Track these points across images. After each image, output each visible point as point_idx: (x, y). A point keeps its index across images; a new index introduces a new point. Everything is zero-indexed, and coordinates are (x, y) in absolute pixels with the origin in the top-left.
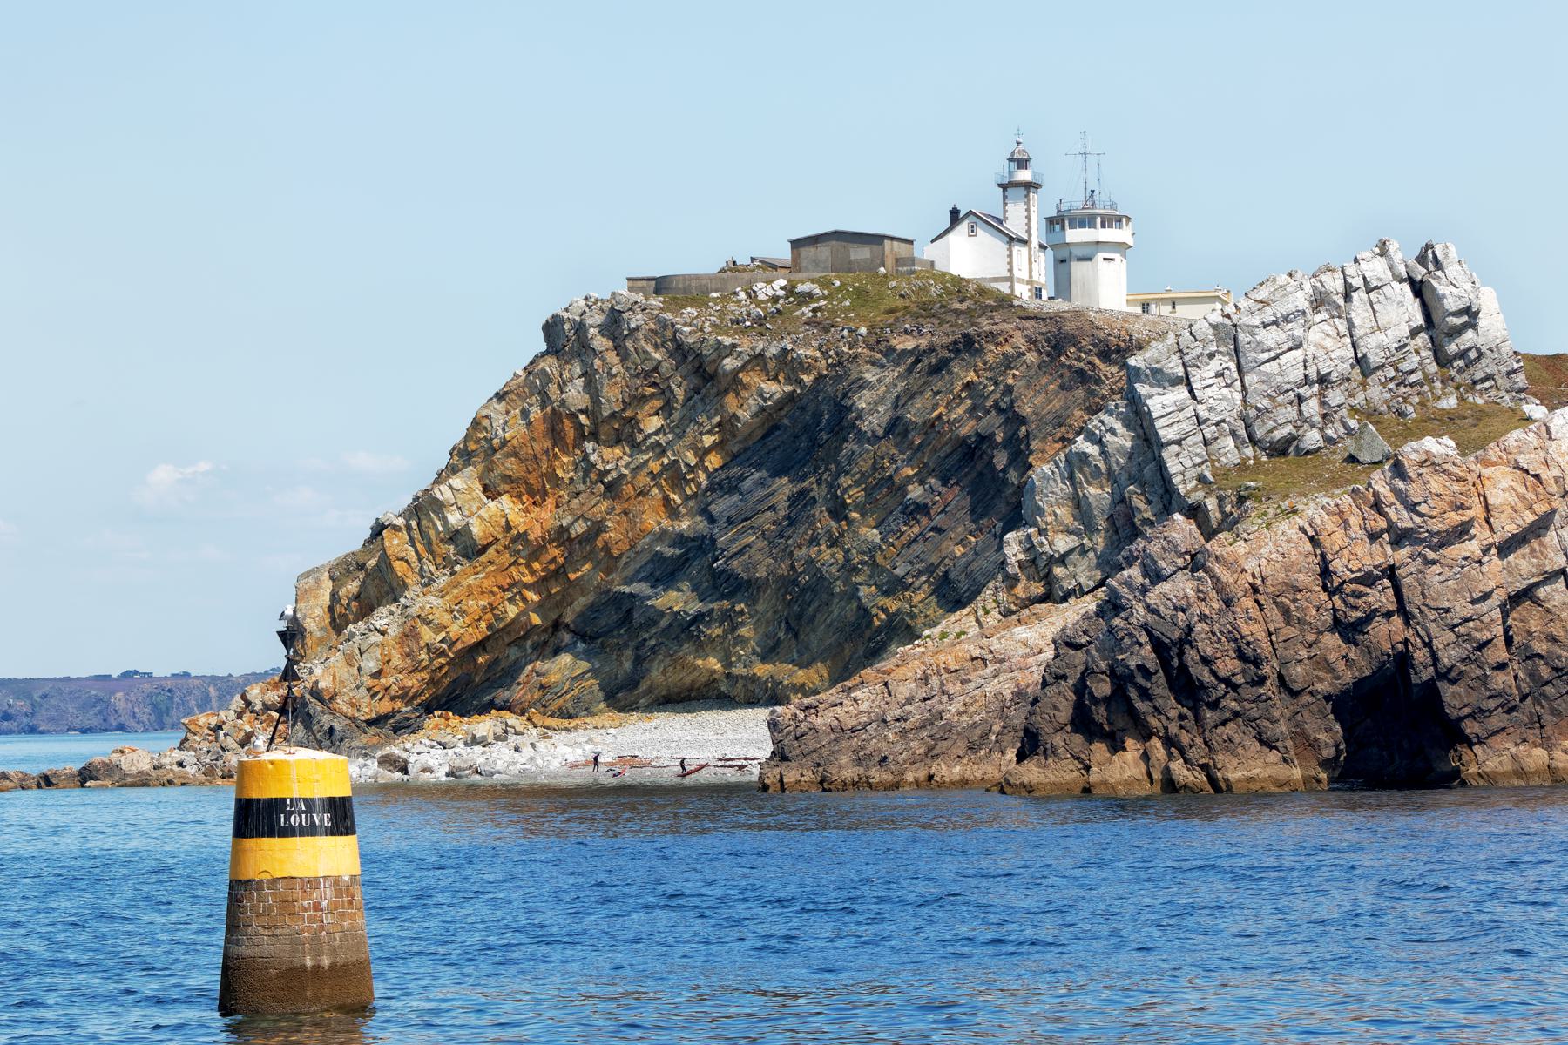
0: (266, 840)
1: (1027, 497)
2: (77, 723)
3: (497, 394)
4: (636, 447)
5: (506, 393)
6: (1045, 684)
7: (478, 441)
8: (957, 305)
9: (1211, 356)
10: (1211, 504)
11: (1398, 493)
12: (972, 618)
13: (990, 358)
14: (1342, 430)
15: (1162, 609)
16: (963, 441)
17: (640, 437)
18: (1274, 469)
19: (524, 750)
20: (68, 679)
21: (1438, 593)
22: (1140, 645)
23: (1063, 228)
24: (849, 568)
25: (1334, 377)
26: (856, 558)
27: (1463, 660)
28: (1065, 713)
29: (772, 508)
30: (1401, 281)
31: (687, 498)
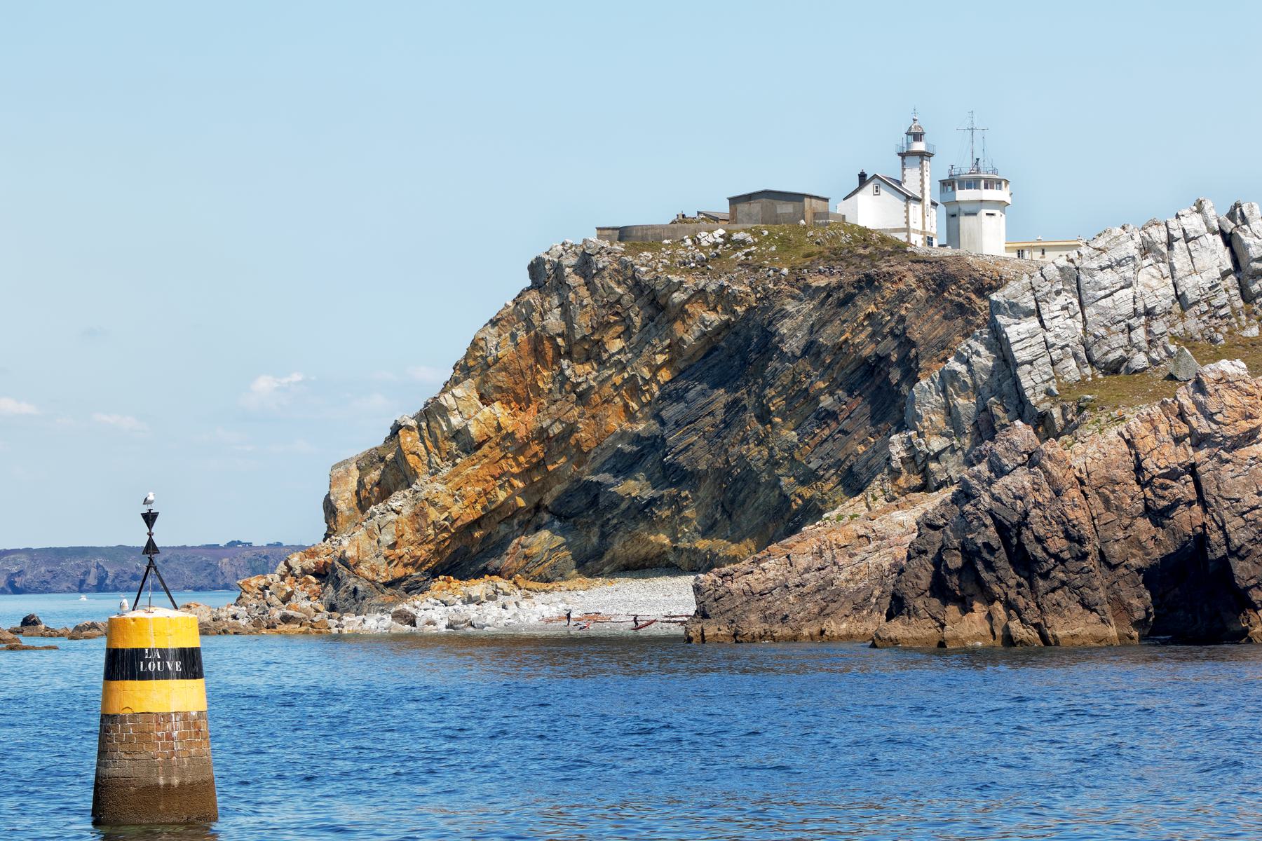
0: (129, 682)
1: (908, 406)
2: (191, 582)
3: (491, 321)
4: (602, 364)
5: (499, 320)
6: (909, 558)
7: (475, 358)
8: (861, 251)
9: (1058, 293)
10: (1056, 412)
11: (1198, 405)
12: (863, 504)
13: (887, 293)
14: (1164, 354)
15: (1004, 497)
16: (865, 361)
17: (605, 356)
18: (1108, 384)
19: (510, 607)
20: (184, 547)
21: (1230, 486)
22: (986, 526)
23: (954, 189)
24: (773, 463)
25: (1158, 310)
26: (779, 455)
27: (1250, 541)
28: (925, 581)
29: (711, 413)
30: (1214, 233)
31: (642, 406)
